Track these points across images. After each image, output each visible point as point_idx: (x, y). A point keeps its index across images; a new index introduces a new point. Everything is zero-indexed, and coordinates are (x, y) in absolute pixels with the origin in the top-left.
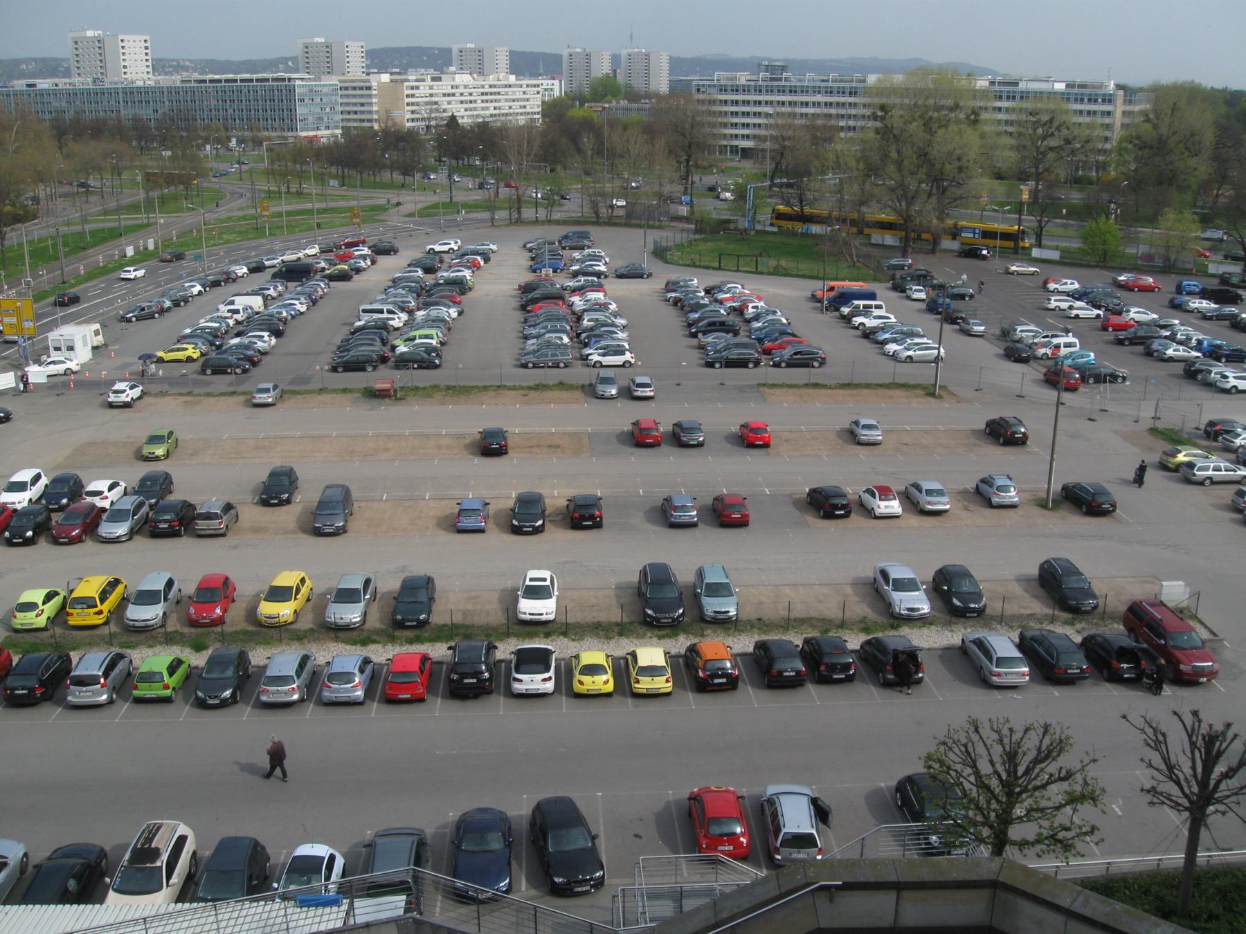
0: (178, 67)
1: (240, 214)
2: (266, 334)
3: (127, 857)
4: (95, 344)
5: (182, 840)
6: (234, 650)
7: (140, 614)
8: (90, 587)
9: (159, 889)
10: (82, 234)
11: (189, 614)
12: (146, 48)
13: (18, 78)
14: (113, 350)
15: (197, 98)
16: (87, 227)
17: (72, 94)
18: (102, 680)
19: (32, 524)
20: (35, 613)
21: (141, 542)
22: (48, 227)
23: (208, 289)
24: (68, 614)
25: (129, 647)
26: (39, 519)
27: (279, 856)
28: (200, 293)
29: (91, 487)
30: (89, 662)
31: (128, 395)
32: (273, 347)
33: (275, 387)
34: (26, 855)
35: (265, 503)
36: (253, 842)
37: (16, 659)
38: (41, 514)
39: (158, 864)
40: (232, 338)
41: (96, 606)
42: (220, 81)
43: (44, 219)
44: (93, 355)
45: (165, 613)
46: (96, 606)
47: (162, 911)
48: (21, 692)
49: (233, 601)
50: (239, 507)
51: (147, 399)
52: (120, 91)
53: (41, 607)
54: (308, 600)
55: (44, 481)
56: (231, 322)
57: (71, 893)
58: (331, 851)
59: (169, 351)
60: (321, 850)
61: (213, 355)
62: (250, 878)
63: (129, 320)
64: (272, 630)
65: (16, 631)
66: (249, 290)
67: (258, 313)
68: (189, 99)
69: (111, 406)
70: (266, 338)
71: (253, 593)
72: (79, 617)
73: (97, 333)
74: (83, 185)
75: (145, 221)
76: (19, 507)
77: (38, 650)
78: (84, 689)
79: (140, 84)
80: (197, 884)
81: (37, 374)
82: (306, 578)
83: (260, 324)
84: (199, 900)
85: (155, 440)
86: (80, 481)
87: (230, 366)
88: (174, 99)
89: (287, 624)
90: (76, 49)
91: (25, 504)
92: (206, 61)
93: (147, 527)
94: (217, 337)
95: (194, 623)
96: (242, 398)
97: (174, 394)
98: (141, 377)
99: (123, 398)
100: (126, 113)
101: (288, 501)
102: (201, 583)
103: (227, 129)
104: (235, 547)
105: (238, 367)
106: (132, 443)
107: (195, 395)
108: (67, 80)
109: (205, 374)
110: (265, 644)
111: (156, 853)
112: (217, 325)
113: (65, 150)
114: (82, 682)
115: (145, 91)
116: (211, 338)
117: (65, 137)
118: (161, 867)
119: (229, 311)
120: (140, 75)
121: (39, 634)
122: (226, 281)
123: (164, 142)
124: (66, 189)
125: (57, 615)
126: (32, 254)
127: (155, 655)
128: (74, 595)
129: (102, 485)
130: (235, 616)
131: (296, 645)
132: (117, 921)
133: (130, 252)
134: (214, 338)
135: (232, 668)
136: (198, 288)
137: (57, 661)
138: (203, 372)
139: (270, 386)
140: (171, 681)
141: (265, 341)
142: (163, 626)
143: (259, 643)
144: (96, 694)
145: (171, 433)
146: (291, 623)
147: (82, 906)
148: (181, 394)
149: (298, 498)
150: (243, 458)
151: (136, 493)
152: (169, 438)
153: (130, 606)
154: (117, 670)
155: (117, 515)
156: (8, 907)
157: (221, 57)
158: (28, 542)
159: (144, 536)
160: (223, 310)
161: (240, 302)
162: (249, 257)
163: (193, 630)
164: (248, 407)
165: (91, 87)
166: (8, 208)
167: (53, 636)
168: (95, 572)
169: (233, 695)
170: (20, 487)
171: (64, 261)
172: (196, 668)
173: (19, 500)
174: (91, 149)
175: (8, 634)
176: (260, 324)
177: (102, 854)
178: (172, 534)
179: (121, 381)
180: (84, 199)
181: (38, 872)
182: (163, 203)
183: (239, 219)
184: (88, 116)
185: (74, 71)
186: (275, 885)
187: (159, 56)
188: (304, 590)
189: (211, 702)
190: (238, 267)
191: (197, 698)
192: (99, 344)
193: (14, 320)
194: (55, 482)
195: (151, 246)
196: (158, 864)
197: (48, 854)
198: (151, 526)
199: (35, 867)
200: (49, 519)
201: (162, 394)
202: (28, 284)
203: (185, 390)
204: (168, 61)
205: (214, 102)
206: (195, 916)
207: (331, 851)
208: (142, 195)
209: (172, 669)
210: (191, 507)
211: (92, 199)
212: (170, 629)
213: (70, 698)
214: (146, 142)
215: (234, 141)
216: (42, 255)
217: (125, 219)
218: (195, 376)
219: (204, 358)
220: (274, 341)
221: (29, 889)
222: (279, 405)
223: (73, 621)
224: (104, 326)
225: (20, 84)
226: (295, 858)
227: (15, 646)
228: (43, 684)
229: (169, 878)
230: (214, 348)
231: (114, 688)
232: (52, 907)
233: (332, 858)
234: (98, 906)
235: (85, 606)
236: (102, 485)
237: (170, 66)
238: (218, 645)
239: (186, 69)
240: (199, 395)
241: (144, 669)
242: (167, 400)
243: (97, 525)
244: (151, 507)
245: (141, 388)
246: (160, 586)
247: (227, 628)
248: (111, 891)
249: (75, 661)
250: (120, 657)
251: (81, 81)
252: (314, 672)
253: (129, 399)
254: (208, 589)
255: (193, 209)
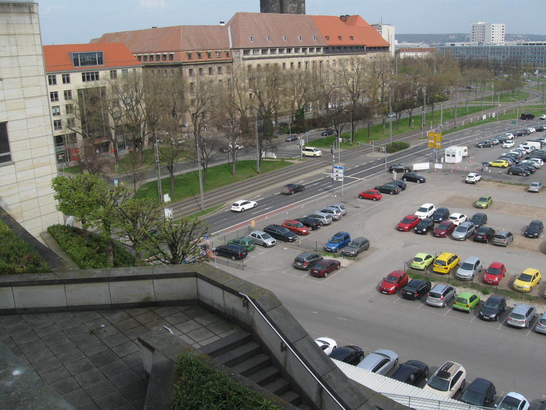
0: (516, 38)
1: (536, 104)
2: (539, 160)
3: (436, 373)
4: (464, 155)
5: (460, 373)
6: (500, 297)
7: (463, 272)
8: (445, 257)
9: (446, 390)
10: (465, 108)
11: (483, 277)
12: (503, 29)
13: (448, 42)
14: (471, 159)
15: (523, 52)
16: (468, 106)
17: (469, 49)
18: (442, 297)
19: (426, 226)
20: (421, 263)
21: (469, 243)
22: (452, 104)
23: (516, 137)
24: (434, 266)
25: (456, 286)
26: (429, 225)
27: (500, 393)
28: (512, 138)
29: (453, 215)
30: (438, 288)
31: (474, 179)
32: (542, 166)
33: (540, 184)
34: (397, 359)
35: (526, 236)
36: (490, 384)
37: (410, 280)
38: (430, 223)
39: (448, 380)
40: (524, 160)
41: (446, 266)
42: (534, 44)
43: (451, 101)
44: (462, 160)
45: (473, 275)
46: (446, 266)
47: (445, 400)
48: (409, 293)
49: (504, 276)
50: (514, 235)
51: (482, 182)
52: (489, 48)
53: (423, 261)
54: (538, 283)
55: (434, 209)
56: (524, 153)
57: (411, 380)
58: (525, 399)
59: (495, 162)
60: (520, 397)
61: (514, 166)
62: (486, 399)
63: (480, 147)
64: (519, 293)
65: (412, 268)
66: (535, 139)
67: (537, 150)
68: (519, 52)
69: (467, 182)
70: (539, 162)
71: (513, 275)
72: (438, 268)
73: (465, 151)
74: (468, 88)
75: (493, 105)
76: (422, 218)
77: (419, 278)
78: (434, 298)
79: (498, 45)
80: (462, 394)
81: (438, 166)
82: (539, 273)
83: (537, 155)
84: (462, 401)
85: (482, 199)
86: (449, 212)
87: (521, 172)
88: (512, 52)
89: (526, 292)
90: (473, 30)
91: (425, 217)
92: (529, 35)
93: (473, 236)
94: (517, 158)
95: (485, 282)
96: (524, 187)
97: (494, 181)
98: (481, 172)
99: (472, 180)
100: (491, 57)
101: (537, 237)
102: (492, 265)
103: (534, 66)
104: (509, 253)
105: (524, 173)
106: (473, 199)
107: (503, 183)
108: (468, 43)
109: (509, 174)
110: (514, 298)
111: (448, 375)
112: (518, 153)
113: (463, 72)
114: (434, 295)
115: (500, 48)
116: (514, 158)
117: (464, 67)
118: (449, 382)
119: (524, 148)
120: (499, 41)
121: (421, 272)
122: (525, 134)
123: (506, 70)
124: (461, 89)
125: (429, 266)
126: (445, 115)
127: (465, 291)
128: (437, 259)
129: (457, 215)
130: (503, 283)
131: (528, 302)
132: (426, 398)
133: (484, 117)
134: (516, 159)
135: (497, 305)
136: (512, 136)
137: (426, 284)
138: (508, 173)
139: (538, 183)
140: (470, 304)
141: (539, 163)
142: (471, 280)
143: (511, 297)
144: (438, 301)
145: (490, 198)
146: (528, 292)
147: (414, 387)
148: (497, 182)
149: (542, 236)
150: (520, 214)
151: (471, 221)
152: (489, 200)
153: (460, 268)
154: (449, 294)
155: (461, 229)
156: (386, 377)
157: (536, 33)
158: (423, 233)
159: (470, 240)
160: (522, 147)
161: (530, 144)
162: (537, 124)
163: (484, 285)
164: (526, 191)
165: (477, 46)
166: (437, 95)
167: (426, 274)
168: (449, 251)
169: (496, 317)
170: (424, 210)
171: (456, 119)
172: (482, 301)
173: (423, 216)
174: (472, 72)
175: (409, 269)
176: (537, 155)
177: (427, 368)
178: (482, 241)
179: (472, 172)
180: (468, 93)
181: (400, 368)
182: (502, 97)
183: (535, 107)
184: (474, 58)
185: (471, 39)
186: (496, 406)
187: (508, 33)
188: (537, 278)
189: (485, 317)
190: (531, 128)
191: (480, 314)
192: (466, 155)
193: (433, 141)
194: (438, 210)
195: (494, 116)
196: (448, 380)
197: (406, 362)
198: (474, 236)
199: (400, 365)
200: (433, 225)
201: (488, 180)
202: (441, 127)
203: (499, 180)
204: (512, 35)
205: (530, 54)
206: (458, 407)
207: (525, 399)
208: (493, 94)
209: (472, 299)
210: (493, 231)
211: (471, 94)
212: (474, 282)
213: (427, 301)
214: (498, 70)
215: (537, 72)
216: (448, 116)
217: (484, 103)
218: (504, 174)
219: (510, 167)
220: (543, 163)
221: (396, 373)
222: (540, 193)
223: (435, 269)
224: (469, 148)
225: (448, 44)
226: (508, 397)
227: (410, 274)
228: (418, 292)
229: (451, 387)
230: (515, 163)
231: (446, 301)
232: (403, 383)
233: (524, 402)
234: (420, 389)
235: (441, 264)
236: (457, 215)
237: (512, 37)
238: (493, 294)
239: (519, 38)
240: (505, 183)
241: (460, 296)
242: (491, 184)
243: (452, 232)
244: (476, 228)
245: (480, 176)
246: (473, 263)
247: (499, 287)
248: (427, 385)
249: (433, 286)
250: (451, 289)
251: (473, 44)
252: (534, 317)
253: (474, 181)
254: (494, 269)
255: (514, 101)
